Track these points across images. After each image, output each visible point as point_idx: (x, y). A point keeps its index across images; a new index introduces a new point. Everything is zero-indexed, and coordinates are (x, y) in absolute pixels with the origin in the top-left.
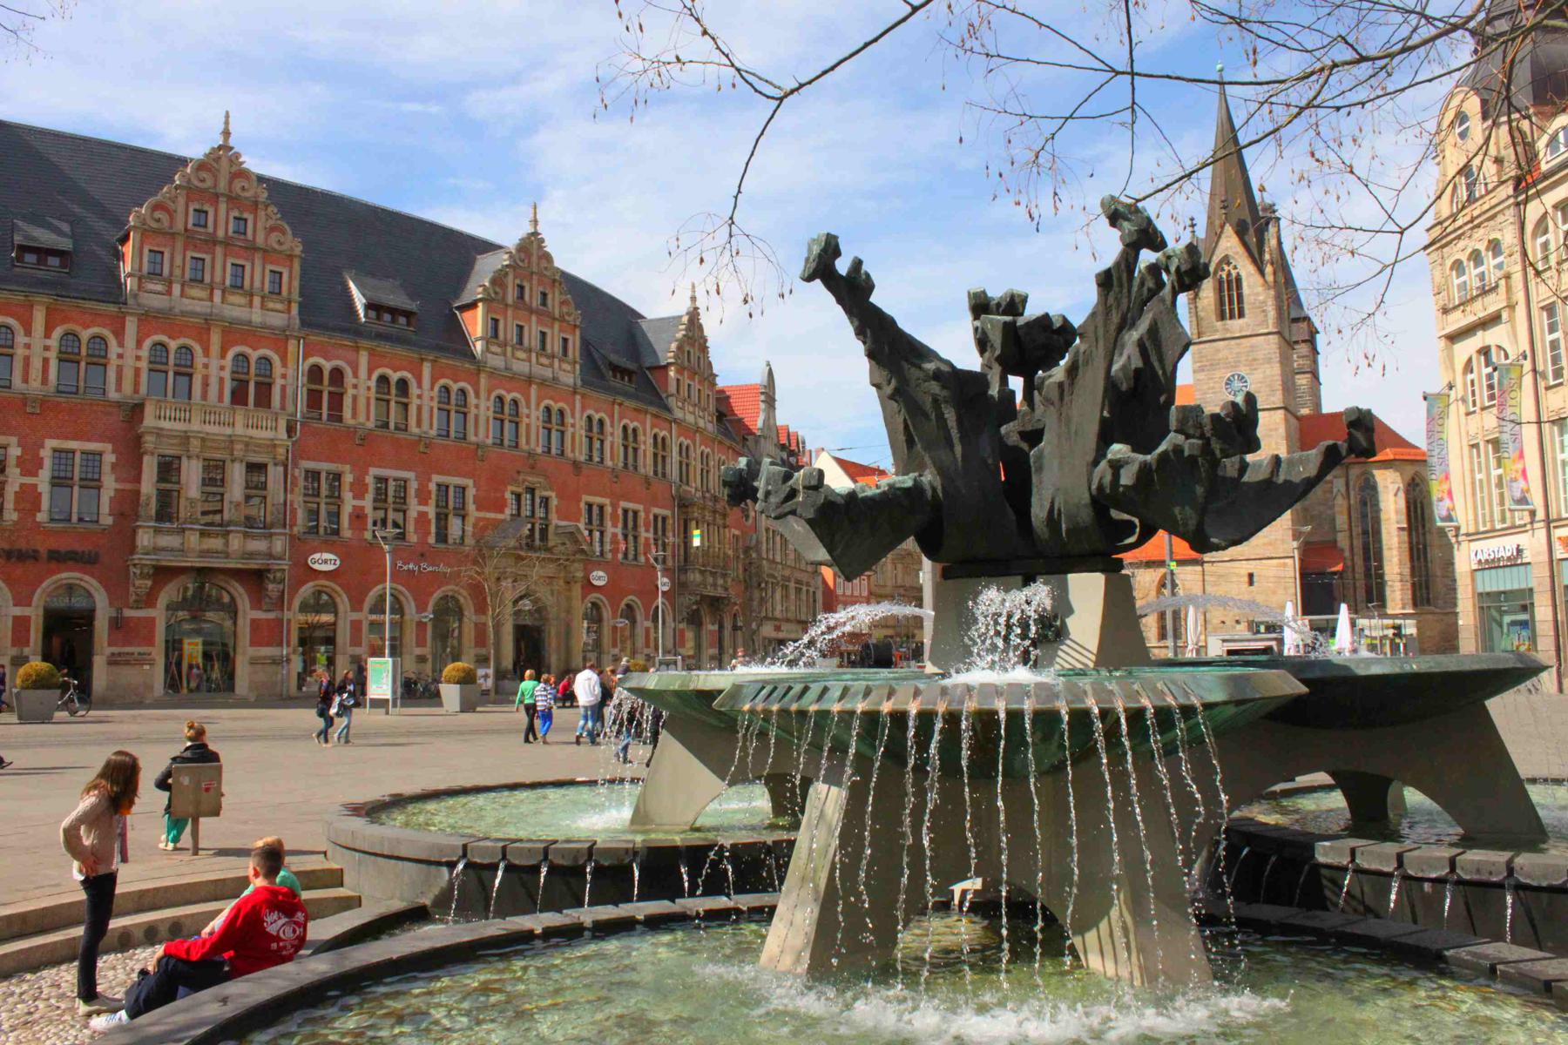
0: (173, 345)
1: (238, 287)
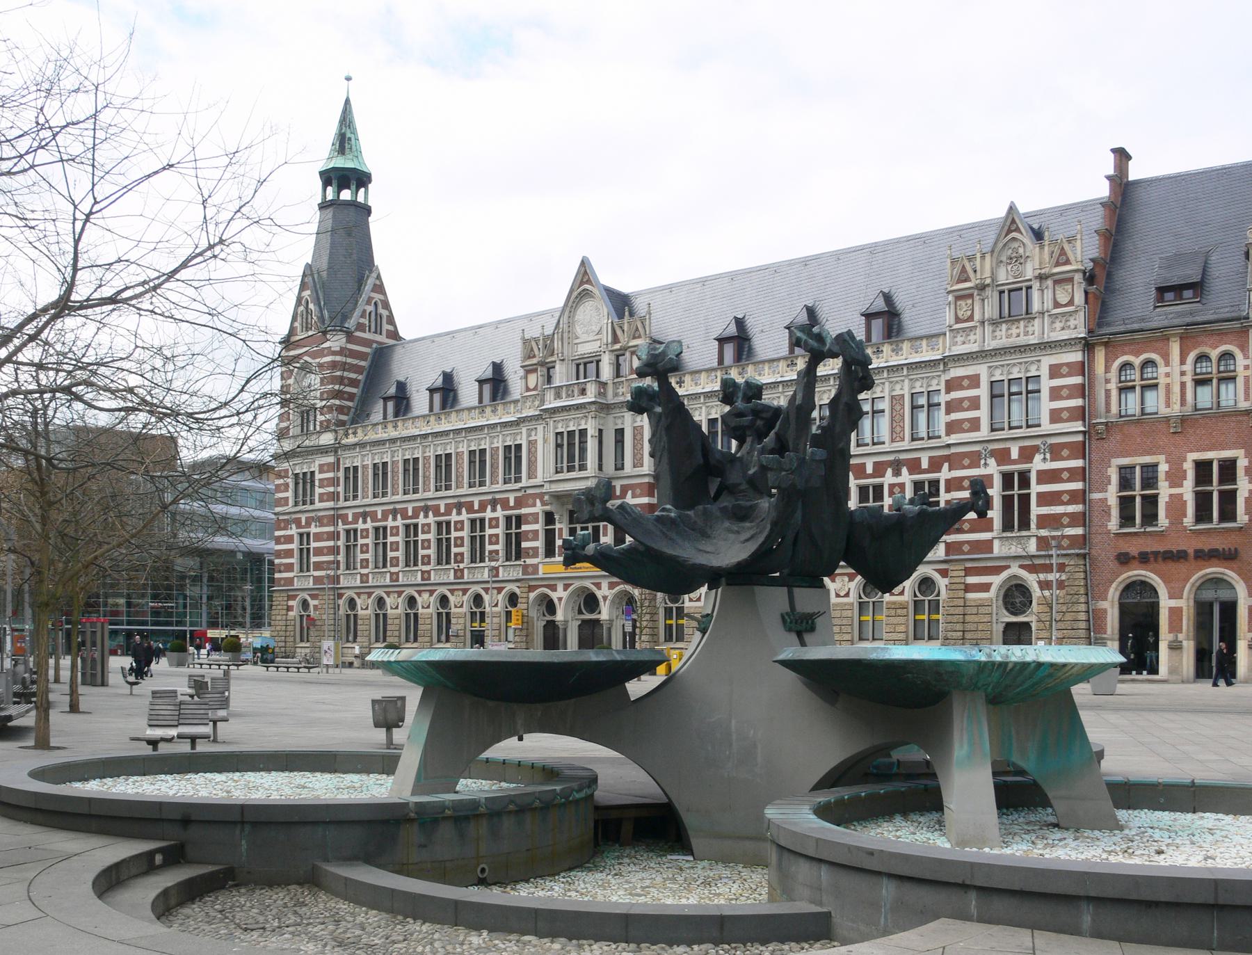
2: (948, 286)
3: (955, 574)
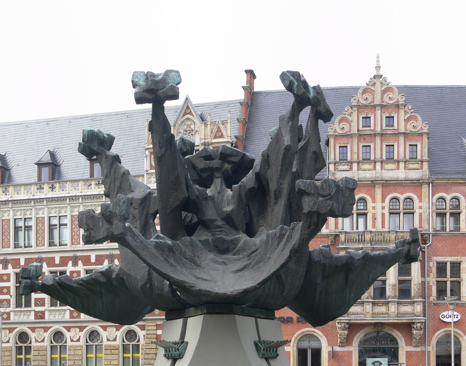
0: (448, 197)
1: (390, 159)
2: (146, 145)
3: (150, 328)
